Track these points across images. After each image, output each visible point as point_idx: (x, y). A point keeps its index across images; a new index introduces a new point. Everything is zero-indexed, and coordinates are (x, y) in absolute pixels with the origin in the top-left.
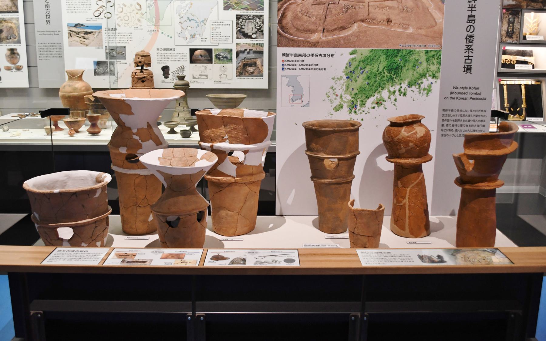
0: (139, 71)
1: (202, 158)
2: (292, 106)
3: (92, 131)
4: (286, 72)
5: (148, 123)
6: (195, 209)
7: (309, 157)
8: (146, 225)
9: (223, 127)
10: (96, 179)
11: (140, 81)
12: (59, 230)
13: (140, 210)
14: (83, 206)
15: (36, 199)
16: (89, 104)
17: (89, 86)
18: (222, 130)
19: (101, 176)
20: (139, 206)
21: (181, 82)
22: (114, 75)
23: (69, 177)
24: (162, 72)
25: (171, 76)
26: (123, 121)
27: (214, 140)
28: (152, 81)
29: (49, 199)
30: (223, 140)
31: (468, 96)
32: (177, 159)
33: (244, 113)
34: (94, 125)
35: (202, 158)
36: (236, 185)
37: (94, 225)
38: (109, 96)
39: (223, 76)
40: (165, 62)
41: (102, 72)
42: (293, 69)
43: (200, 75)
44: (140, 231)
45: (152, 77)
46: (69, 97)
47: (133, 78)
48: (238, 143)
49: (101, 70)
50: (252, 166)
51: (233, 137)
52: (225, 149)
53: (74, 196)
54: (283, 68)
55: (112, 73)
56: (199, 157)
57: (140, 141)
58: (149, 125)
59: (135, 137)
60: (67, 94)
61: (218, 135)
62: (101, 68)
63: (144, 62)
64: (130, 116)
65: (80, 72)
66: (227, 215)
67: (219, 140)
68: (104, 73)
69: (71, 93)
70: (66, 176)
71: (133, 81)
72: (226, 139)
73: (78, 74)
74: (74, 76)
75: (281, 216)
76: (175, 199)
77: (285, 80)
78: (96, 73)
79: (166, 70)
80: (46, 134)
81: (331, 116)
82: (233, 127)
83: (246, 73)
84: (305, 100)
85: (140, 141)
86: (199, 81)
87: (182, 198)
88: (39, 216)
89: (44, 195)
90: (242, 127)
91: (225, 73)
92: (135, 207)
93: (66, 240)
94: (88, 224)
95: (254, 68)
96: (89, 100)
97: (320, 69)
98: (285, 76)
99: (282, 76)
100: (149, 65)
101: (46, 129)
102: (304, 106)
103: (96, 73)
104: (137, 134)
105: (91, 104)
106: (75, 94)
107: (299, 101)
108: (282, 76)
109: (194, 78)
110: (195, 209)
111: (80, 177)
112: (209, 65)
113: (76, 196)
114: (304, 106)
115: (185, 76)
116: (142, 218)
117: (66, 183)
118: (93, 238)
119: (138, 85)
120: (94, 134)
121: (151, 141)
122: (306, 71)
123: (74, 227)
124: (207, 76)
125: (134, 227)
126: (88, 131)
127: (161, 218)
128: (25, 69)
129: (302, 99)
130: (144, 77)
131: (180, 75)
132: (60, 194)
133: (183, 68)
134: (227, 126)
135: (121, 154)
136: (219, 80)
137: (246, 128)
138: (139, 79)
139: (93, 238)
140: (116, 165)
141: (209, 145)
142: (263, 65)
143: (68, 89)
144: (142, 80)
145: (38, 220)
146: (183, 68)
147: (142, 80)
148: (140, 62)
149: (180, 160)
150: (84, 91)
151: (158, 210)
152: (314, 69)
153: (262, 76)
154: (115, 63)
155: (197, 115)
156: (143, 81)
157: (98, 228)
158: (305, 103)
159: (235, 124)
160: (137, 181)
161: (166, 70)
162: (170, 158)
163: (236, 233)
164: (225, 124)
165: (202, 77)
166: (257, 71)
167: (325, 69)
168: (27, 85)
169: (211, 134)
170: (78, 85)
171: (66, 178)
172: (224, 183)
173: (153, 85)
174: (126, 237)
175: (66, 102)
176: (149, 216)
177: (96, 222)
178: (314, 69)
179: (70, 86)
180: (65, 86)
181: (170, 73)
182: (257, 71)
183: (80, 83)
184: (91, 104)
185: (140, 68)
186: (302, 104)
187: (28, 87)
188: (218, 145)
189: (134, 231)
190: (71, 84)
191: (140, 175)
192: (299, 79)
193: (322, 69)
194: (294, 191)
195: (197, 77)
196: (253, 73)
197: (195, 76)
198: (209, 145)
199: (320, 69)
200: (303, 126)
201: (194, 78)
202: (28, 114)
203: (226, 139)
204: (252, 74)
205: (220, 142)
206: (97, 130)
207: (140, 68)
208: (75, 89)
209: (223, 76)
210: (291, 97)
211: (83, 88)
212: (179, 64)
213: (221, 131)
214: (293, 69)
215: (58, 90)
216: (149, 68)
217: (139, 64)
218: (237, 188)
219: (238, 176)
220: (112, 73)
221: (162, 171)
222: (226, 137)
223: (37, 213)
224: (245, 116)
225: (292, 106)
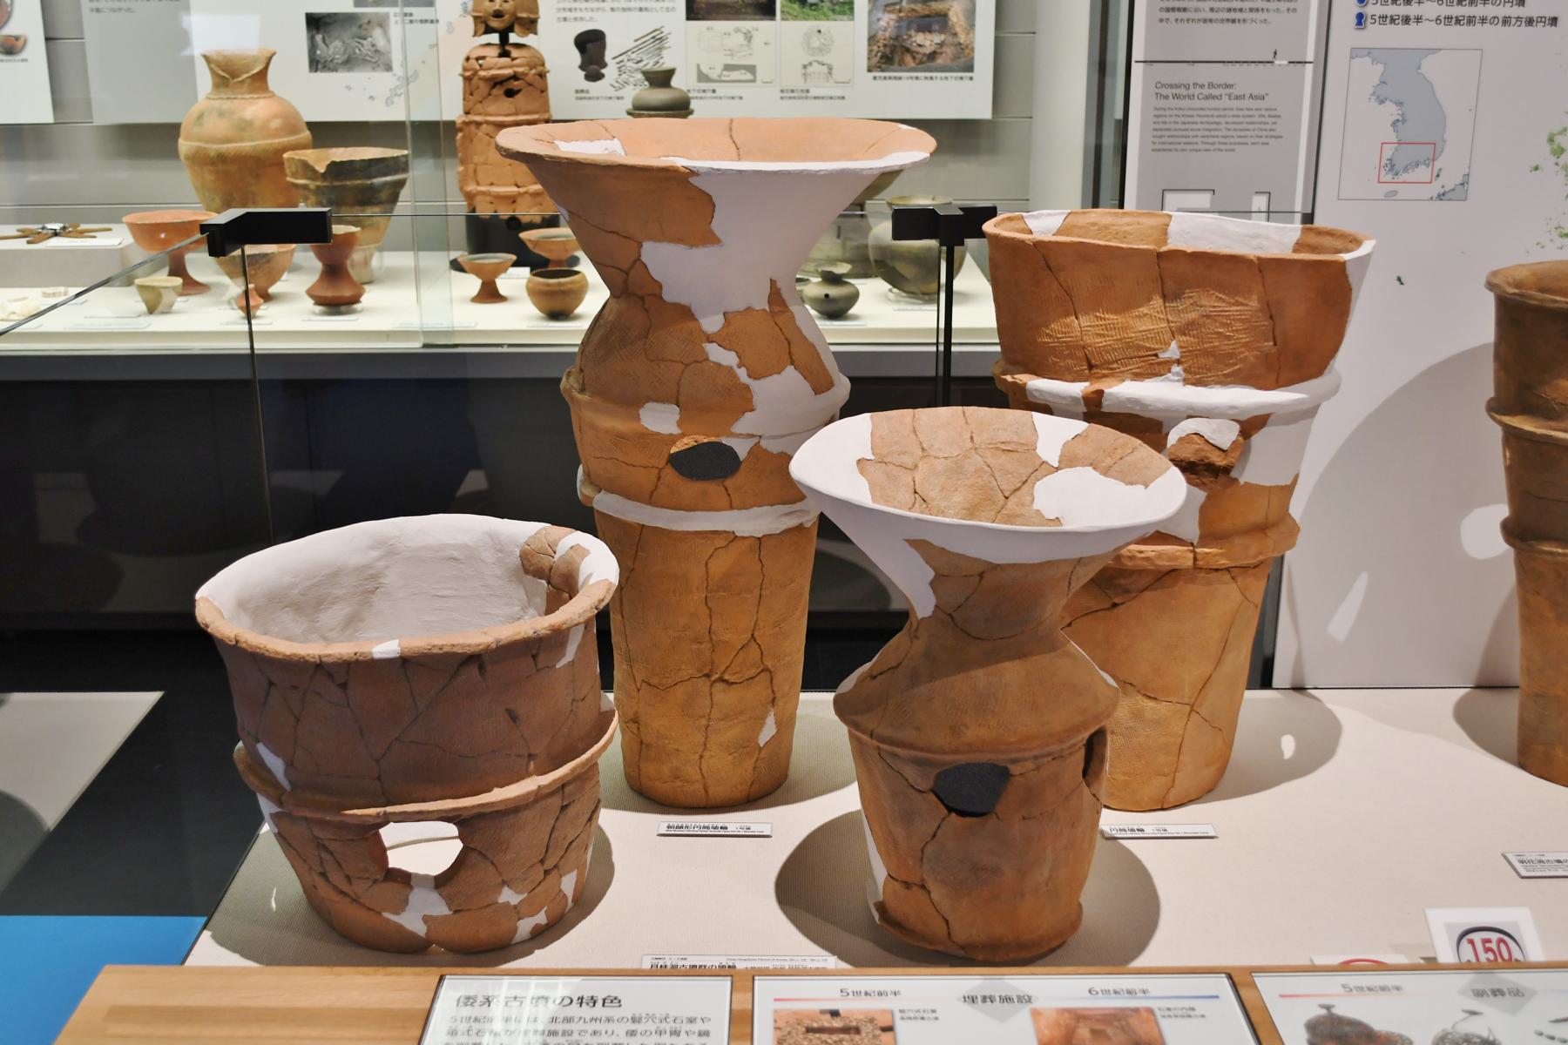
0: (495, 52)
1: (1069, 459)
2: (1390, 195)
3: (329, 293)
4: (1376, 34)
5: (773, 282)
6: (1077, 729)
7: (1513, 437)
8: (749, 764)
9: (1157, 302)
10: (525, 557)
11: (498, 91)
12: (389, 834)
13: (725, 698)
14: (513, 716)
15: (271, 684)
16: (305, 187)
17: (297, 115)
18: (1148, 319)
19: (553, 547)
20: (721, 680)
21: (660, 96)
22: (389, 68)
23: (390, 550)
24: (575, 57)
25: (610, 71)
26: (656, 274)
27: (1106, 364)
28: (544, 90)
29: (343, 686)
30: (1153, 368)
31: (1249, 140)
32: (940, 465)
33: (1173, 228)
34: (334, 271)
35: (1069, 459)
36: (1193, 580)
37: (556, 801)
38: (556, 147)
39: (816, 68)
40: (587, 15)
41: (339, 58)
42: (1407, 20)
43: (728, 68)
44: (718, 792)
45: (542, 75)
46: (222, 159)
47: (467, 80)
48: (1225, 381)
49: (334, 48)
50: (1270, 489)
51: (1206, 353)
52: (1160, 410)
53: (474, 671)
54: (1360, 17)
55: (381, 61)
56: (1049, 451)
57: (742, 374)
58: (776, 297)
59: (716, 353)
60: (214, 148)
61: (1129, 345)
62: (337, 43)
63: (514, 15)
64: (701, 253)
65: (256, 60)
66: (1137, 715)
67: (1134, 366)
68: (349, 63)
69: (228, 141)
70: (378, 543)
71: (469, 92)
72: (1168, 363)
73: (247, 68)
74: (234, 75)
75: (1299, 689)
76: (980, 676)
77: (1369, 73)
78: (316, 64)
79: (591, 46)
80: (143, 307)
81: (1559, 241)
82: (1211, 302)
83: (908, 58)
84: (1451, 167)
85: (742, 374)
86: (722, 90)
87: (1012, 672)
88: (290, 765)
89: (320, 669)
90: (1254, 303)
91: (825, 59)
92: (703, 685)
93: (425, 877)
94: (539, 796)
95: (938, 38)
96: (307, 169)
97: (1530, 22)
98: (1369, 52)
99: (1355, 53)
100: (530, 25)
101: (142, 288)
102: (1441, 197)
103: (316, 64)
104: (723, 339)
105: (312, 184)
106: (246, 146)
107: (1423, 173)
108: (1355, 53)
109: (702, 77)
110: (1077, 729)
111: (444, 547)
112: (761, 27)
113: (481, 668)
114: (1441, 197)
115: (671, 72)
116: (731, 733)
117: (374, 577)
118: (549, 864)
119: (491, 109)
120: (335, 306)
121: (790, 369)
122: (1464, 29)
123: (465, 823)
124: (751, 69)
125: (693, 773)
126: (310, 293)
127: (910, 772)
128: (36, 49)
129: (1438, 164)
130: (515, 77)
131: (649, 64)
132: (405, 663)
133: (657, 40)
134: (1177, 296)
135: (647, 438)
136: (799, 84)
137: (1270, 310)
138: (496, 82)
139: (549, 864)
140: (611, 491)
141: (1077, 389)
142: (972, 26)
143: (216, 126)
144: (507, 87)
145: (275, 784)
146: (657, 40)
147: (507, 87)
148: (498, 14)
149: (956, 470)
150: (276, 133)
151: (887, 732)
152: (1506, 21)
153: (970, 68)
154: (392, 20)
155: (995, 240)
156: (510, 93)
157: (571, 811)
158: (1450, 180)
159: (1221, 287)
160: (720, 565)
161: (591, 46)
162: (907, 460)
163: (1172, 799)
164: (1170, 286)
165: (735, 75)
166: (949, 51)
167: (1554, 21)
168: (45, 115)
169: (1088, 340)
170: (255, 109)
171: (375, 554)
172: (1141, 572)
173: (545, 107)
174: (662, 821)
175: (209, 177)
176: (761, 721)
177: (561, 786)
178: (1506, 21)
179: (221, 114)
180: (201, 116)
181: (608, 58)
182: (949, 51)
183: (262, 102)
184: (312, 184)
185: (494, 38)
186: (1436, 189)
187: (51, 120)
188: (1125, 390)
189: (694, 791)
190: (227, 105)
191: (733, 538)
192: (1429, 66)
193: (1542, 19)
194: (1361, 584)
195: (713, 75)
196: (932, 56)
197: (705, 70)
198: (1077, 389)
199: (1530, 22)
200: (1491, 286)
201: (702, 77)
202: (57, 226)
203: (1168, 363)
204: (929, 61)
205: (1139, 376)
206: (347, 293)
207: (494, 38)
208: (245, 126)
209: (816, 68)
210: (1388, 152)
211: (276, 124)
212: (641, 25)
213: (1144, 325)
214: (1407, 20)
215: (172, 130)
216: (529, 40)
217: (495, 23)
218: (1195, 590)
219: (1209, 536)
220: (381, 61)
221: (938, 542)
222: (1173, 351)
223: (276, 752)
224: (1173, 244)
225: (1390, 195)
